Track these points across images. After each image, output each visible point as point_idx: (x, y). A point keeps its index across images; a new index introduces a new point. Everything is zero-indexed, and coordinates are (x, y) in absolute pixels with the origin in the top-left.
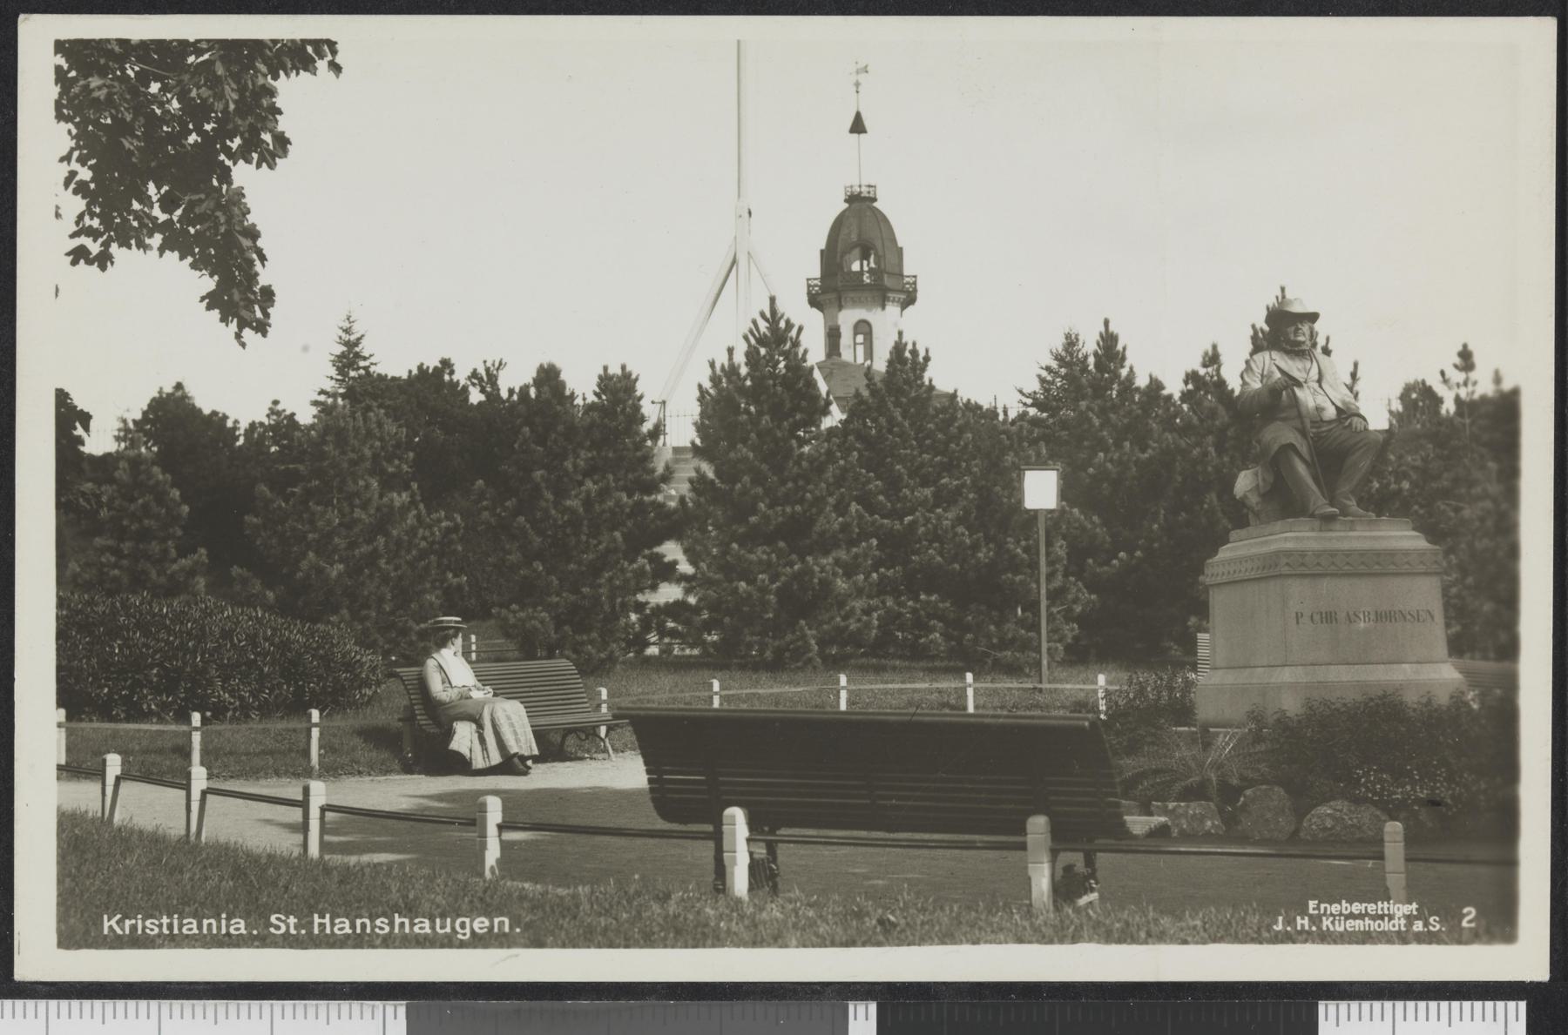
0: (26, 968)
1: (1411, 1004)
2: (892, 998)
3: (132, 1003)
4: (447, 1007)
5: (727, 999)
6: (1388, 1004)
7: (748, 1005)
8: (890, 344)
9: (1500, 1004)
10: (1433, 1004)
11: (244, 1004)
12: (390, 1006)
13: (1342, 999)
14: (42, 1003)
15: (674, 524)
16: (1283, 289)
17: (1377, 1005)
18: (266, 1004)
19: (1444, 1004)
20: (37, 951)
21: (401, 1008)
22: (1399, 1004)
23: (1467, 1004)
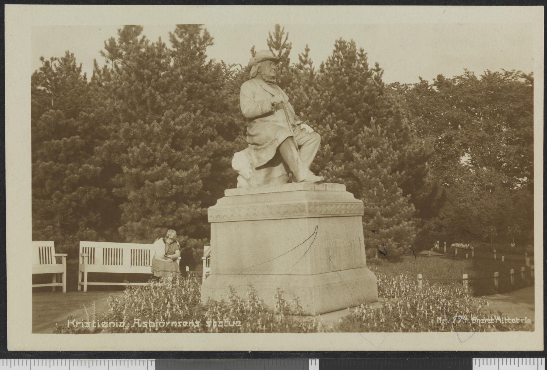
0: (11, 346)
1: (505, 359)
2: (326, 358)
3: (60, 360)
4: (170, 361)
5: (279, 358)
6: (497, 359)
7: (274, 360)
8: (168, 38)
9: (536, 359)
10: (512, 359)
11: (99, 360)
12: (150, 361)
13: (481, 357)
14: (29, 360)
15: (173, 100)
16: (307, 50)
17: (493, 359)
18: (107, 360)
19: (516, 359)
20: (20, 332)
21: (153, 361)
22: (501, 359)
23: (524, 359)
